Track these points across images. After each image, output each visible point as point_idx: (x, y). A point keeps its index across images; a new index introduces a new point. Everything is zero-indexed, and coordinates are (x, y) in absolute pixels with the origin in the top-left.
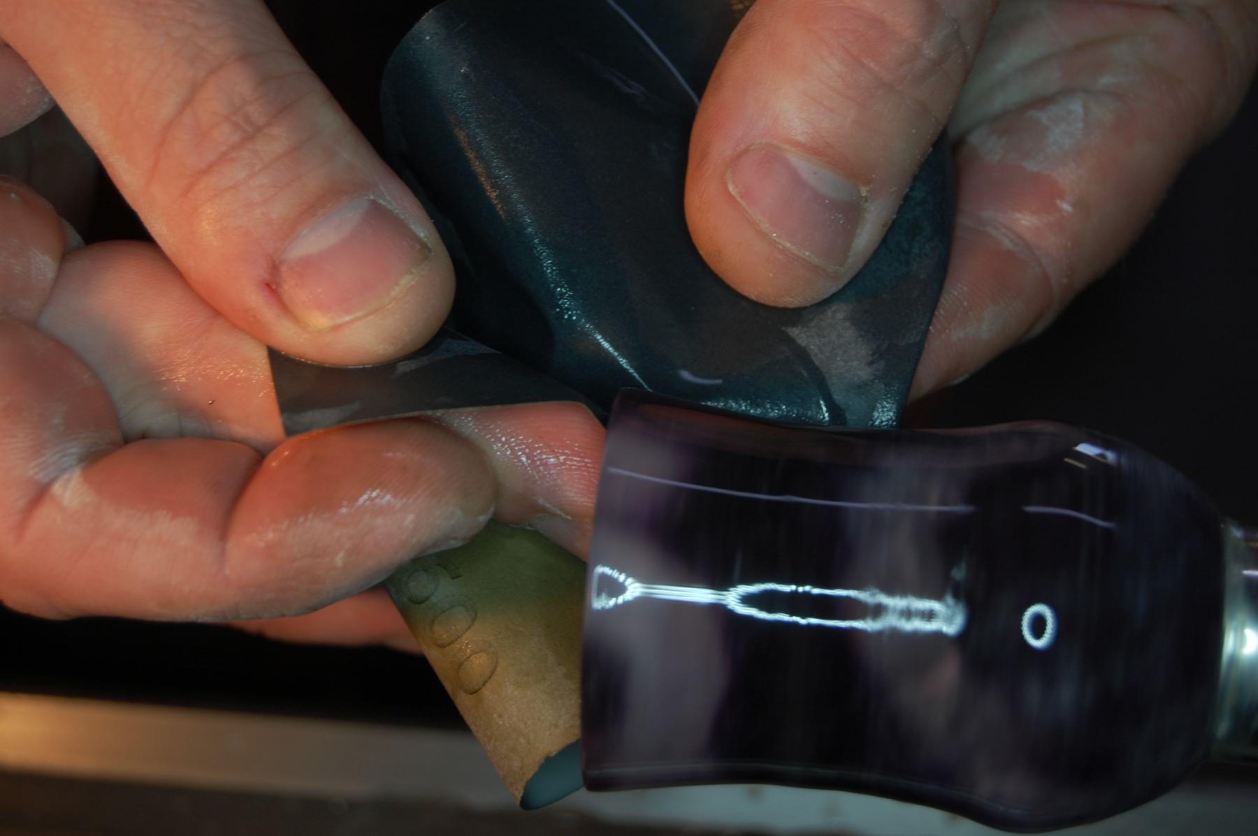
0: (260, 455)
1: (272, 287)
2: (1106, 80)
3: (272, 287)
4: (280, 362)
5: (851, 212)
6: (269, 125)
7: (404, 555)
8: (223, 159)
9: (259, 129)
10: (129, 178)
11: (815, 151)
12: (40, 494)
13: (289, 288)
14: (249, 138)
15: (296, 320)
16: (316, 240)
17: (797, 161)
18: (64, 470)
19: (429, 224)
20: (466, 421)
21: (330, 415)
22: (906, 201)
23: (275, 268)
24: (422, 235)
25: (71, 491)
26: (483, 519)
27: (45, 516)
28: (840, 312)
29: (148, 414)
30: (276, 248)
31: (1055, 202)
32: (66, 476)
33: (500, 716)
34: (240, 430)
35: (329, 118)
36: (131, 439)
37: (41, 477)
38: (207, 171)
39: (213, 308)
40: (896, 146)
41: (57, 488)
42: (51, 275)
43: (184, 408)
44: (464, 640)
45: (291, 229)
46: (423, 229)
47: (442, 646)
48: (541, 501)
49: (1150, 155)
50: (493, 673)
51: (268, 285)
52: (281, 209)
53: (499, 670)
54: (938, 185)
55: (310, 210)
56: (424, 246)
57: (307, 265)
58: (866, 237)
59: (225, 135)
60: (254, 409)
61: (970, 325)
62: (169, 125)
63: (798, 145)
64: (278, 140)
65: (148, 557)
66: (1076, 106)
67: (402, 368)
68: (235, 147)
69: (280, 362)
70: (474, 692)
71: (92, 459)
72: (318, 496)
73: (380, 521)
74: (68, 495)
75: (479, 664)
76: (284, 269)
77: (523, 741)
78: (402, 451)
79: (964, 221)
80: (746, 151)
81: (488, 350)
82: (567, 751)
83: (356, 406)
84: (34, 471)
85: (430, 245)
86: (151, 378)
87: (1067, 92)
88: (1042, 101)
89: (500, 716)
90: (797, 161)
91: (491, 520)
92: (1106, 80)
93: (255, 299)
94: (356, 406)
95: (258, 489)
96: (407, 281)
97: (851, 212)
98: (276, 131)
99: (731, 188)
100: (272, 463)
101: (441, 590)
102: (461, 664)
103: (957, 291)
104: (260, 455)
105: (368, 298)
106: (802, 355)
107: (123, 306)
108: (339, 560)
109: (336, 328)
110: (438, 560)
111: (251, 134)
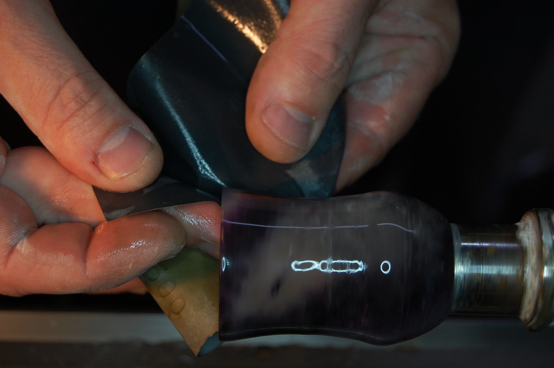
0: (93, 228)
1: (95, 163)
2: (400, 67)
3: (95, 163)
4: (99, 192)
5: (309, 126)
6: (89, 101)
7: (154, 263)
8: (72, 115)
9: (86, 103)
10: (34, 123)
11: (296, 104)
12: (12, 249)
13: (101, 164)
14: (83, 106)
15: (105, 176)
16: (110, 145)
17: (288, 108)
18: (20, 240)
19: (151, 134)
20: (171, 210)
21: (124, 212)
22: (328, 121)
23: (96, 156)
24: (150, 139)
25: (24, 247)
26: (182, 246)
27: (15, 258)
28: (306, 164)
29: (45, 215)
30: (87, 145)
31: (384, 112)
32: (21, 242)
33: (189, 322)
34: (82, 218)
35: (111, 96)
36: (41, 225)
37: (12, 243)
38: (68, 120)
39: (68, 171)
40: (325, 99)
41: (18, 247)
42: (4, 163)
43: (60, 211)
44: (172, 293)
45: (101, 141)
46: (150, 136)
47: (164, 297)
48: (202, 238)
49: (416, 95)
50: (184, 306)
51: (94, 163)
52: (97, 133)
53: (187, 304)
54: (339, 114)
55: (108, 133)
56: (151, 143)
57: (109, 154)
58: (315, 135)
59: (73, 106)
60: (91, 210)
61: (355, 163)
62: (51, 103)
63: (289, 103)
64: (93, 107)
65: (58, 270)
66: (389, 78)
67: (146, 191)
68: (78, 110)
69: (99, 192)
70: (178, 313)
71: (29, 234)
72: (121, 242)
73: (145, 250)
74: (23, 249)
75: (179, 302)
76: (99, 156)
77: (198, 331)
78: (150, 223)
79: (350, 125)
80: (269, 106)
81: (175, 181)
82: (215, 335)
83: (132, 208)
84: (9, 241)
85: (153, 143)
86: (46, 200)
87: (385, 72)
88: (376, 76)
89: (189, 322)
90: (288, 108)
91: (185, 247)
92: (400, 67)
93: (89, 169)
94: (132, 208)
95: (95, 242)
96: (147, 158)
97: (309, 126)
98: (92, 103)
99: (264, 120)
100: (99, 231)
101: (163, 275)
102: (171, 303)
103: (349, 152)
104: (93, 228)
105: (130, 166)
106: (293, 181)
107: (34, 172)
108: (130, 266)
109: (122, 178)
110: (163, 264)
111: (83, 105)
